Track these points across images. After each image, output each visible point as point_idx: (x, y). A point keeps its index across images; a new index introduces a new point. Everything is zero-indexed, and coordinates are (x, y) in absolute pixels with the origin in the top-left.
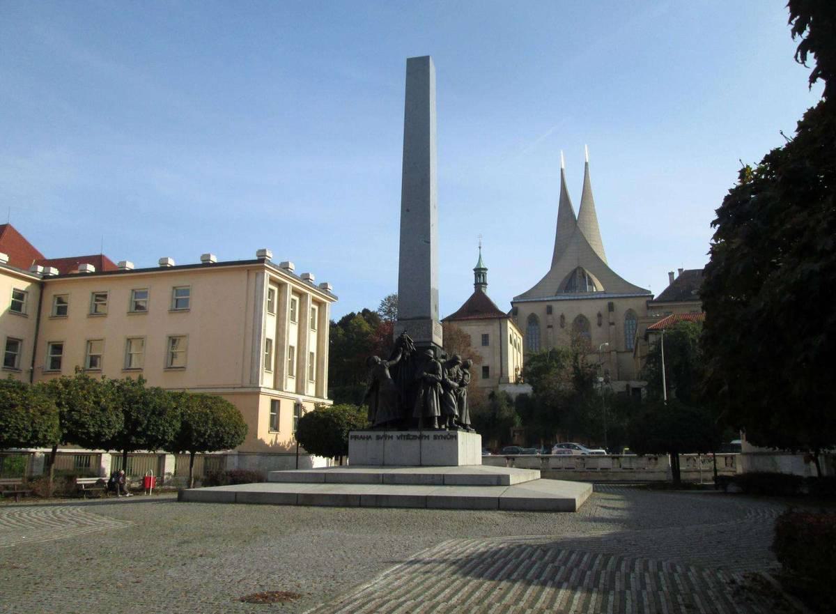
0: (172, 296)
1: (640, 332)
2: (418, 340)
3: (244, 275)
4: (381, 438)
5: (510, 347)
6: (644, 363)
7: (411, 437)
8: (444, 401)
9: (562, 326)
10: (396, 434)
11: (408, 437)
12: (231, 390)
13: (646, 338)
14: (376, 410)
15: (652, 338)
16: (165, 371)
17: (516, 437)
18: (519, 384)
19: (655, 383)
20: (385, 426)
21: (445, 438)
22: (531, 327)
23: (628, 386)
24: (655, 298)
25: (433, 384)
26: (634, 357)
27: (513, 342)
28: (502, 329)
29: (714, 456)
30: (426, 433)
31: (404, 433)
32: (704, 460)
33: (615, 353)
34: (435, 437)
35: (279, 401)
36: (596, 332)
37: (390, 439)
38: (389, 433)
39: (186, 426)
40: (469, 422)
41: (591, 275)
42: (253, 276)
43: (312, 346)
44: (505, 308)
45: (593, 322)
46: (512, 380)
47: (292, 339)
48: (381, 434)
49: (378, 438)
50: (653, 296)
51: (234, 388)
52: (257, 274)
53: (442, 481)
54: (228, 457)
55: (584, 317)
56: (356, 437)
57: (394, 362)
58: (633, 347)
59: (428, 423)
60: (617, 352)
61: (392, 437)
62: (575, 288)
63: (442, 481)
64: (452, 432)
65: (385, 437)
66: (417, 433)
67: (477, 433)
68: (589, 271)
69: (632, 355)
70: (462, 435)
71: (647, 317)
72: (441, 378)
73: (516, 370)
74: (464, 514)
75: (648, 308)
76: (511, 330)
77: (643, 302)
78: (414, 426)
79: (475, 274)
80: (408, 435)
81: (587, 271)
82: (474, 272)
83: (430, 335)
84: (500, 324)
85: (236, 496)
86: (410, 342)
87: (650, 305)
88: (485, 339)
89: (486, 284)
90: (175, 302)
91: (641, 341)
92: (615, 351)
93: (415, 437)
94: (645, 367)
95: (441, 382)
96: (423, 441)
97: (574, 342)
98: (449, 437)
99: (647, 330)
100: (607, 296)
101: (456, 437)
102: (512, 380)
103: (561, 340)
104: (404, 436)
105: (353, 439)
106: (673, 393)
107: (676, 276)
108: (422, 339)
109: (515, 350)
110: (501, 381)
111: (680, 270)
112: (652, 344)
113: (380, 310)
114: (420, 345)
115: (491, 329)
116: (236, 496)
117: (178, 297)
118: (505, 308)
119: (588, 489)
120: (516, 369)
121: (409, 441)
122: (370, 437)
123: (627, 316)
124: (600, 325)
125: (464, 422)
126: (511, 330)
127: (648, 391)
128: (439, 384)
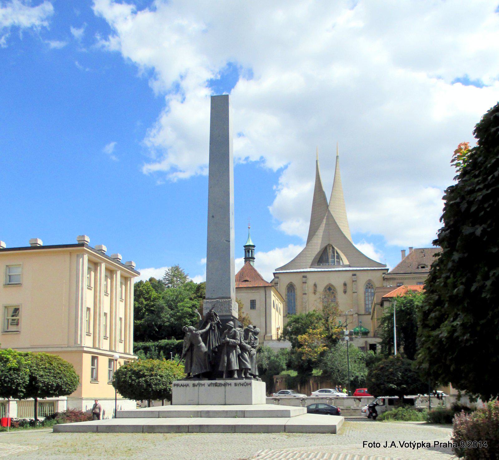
0: (6, 273)
1: (377, 300)
2: (221, 314)
3: (67, 258)
4: (197, 386)
5: (273, 311)
6: (380, 324)
7: (218, 385)
8: (240, 357)
9: (315, 293)
10: (207, 382)
11: (216, 385)
12: (60, 349)
13: (382, 305)
14: (191, 366)
15: (386, 304)
16: (3, 334)
17: (278, 384)
18: (281, 341)
19: (388, 343)
20: (198, 377)
21: (242, 385)
22: (290, 296)
23: (366, 342)
24: (389, 271)
25: (234, 347)
26: (372, 319)
27: (275, 307)
28: (267, 296)
29: (430, 397)
30: (229, 381)
31: (213, 382)
32: (423, 400)
33: (357, 315)
34: (236, 385)
35: (97, 357)
36: (341, 298)
37: (230, 386)
38: (202, 382)
39: (33, 379)
40: (257, 374)
41: (339, 251)
42: (74, 257)
43: (121, 314)
44: (268, 277)
45: (340, 289)
46: (274, 337)
47: (106, 308)
48: (197, 382)
49: (194, 385)
50: (388, 270)
51: (62, 347)
52: (78, 256)
53: (243, 414)
54: (59, 402)
55: (332, 286)
56: (177, 385)
57: (204, 330)
58: (371, 311)
59: (230, 374)
60: (359, 315)
61: (231, 384)
62: (327, 261)
63: (243, 414)
64: (248, 381)
65: (199, 385)
67: (263, 381)
68: (338, 248)
69: (370, 317)
70: (254, 382)
71: (383, 287)
72: (239, 342)
73: (278, 329)
74: (263, 436)
75: (384, 279)
76: (274, 298)
77: (379, 275)
78: (219, 376)
79: (245, 250)
80: (216, 383)
81: (335, 248)
82: (244, 248)
83: (230, 310)
84: (265, 292)
85: (97, 428)
86: (216, 316)
87: (386, 276)
89: (254, 258)
90: (8, 277)
91: (378, 307)
92: (356, 313)
93: (220, 385)
94: (380, 327)
95: (239, 345)
96: (227, 387)
97: (325, 307)
98: (245, 384)
99: (383, 298)
101: (250, 384)
102: (274, 337)
103: (311, 304)
104: (213, 384)
105: (176, 387)
106: (402, 350)
107: (407, 253)
108: (225, 314)
109: (277, 313)
110: (266, 338)
111: (411, 248)
112: (386, 308)
113: (164, 279)
114: (224, 318)
115: (258, 296)
116: (97, 428)
117: (11, 274)
118: (268, 277)
119: (341, 419)
120: (277, 328)
121: (216, 387)
122: (188, 385)
123: (367, 286)
124: (345, 292)
125: (254, 374)
126: (274, 298)
127: (382, 347)
128: (238, 347)
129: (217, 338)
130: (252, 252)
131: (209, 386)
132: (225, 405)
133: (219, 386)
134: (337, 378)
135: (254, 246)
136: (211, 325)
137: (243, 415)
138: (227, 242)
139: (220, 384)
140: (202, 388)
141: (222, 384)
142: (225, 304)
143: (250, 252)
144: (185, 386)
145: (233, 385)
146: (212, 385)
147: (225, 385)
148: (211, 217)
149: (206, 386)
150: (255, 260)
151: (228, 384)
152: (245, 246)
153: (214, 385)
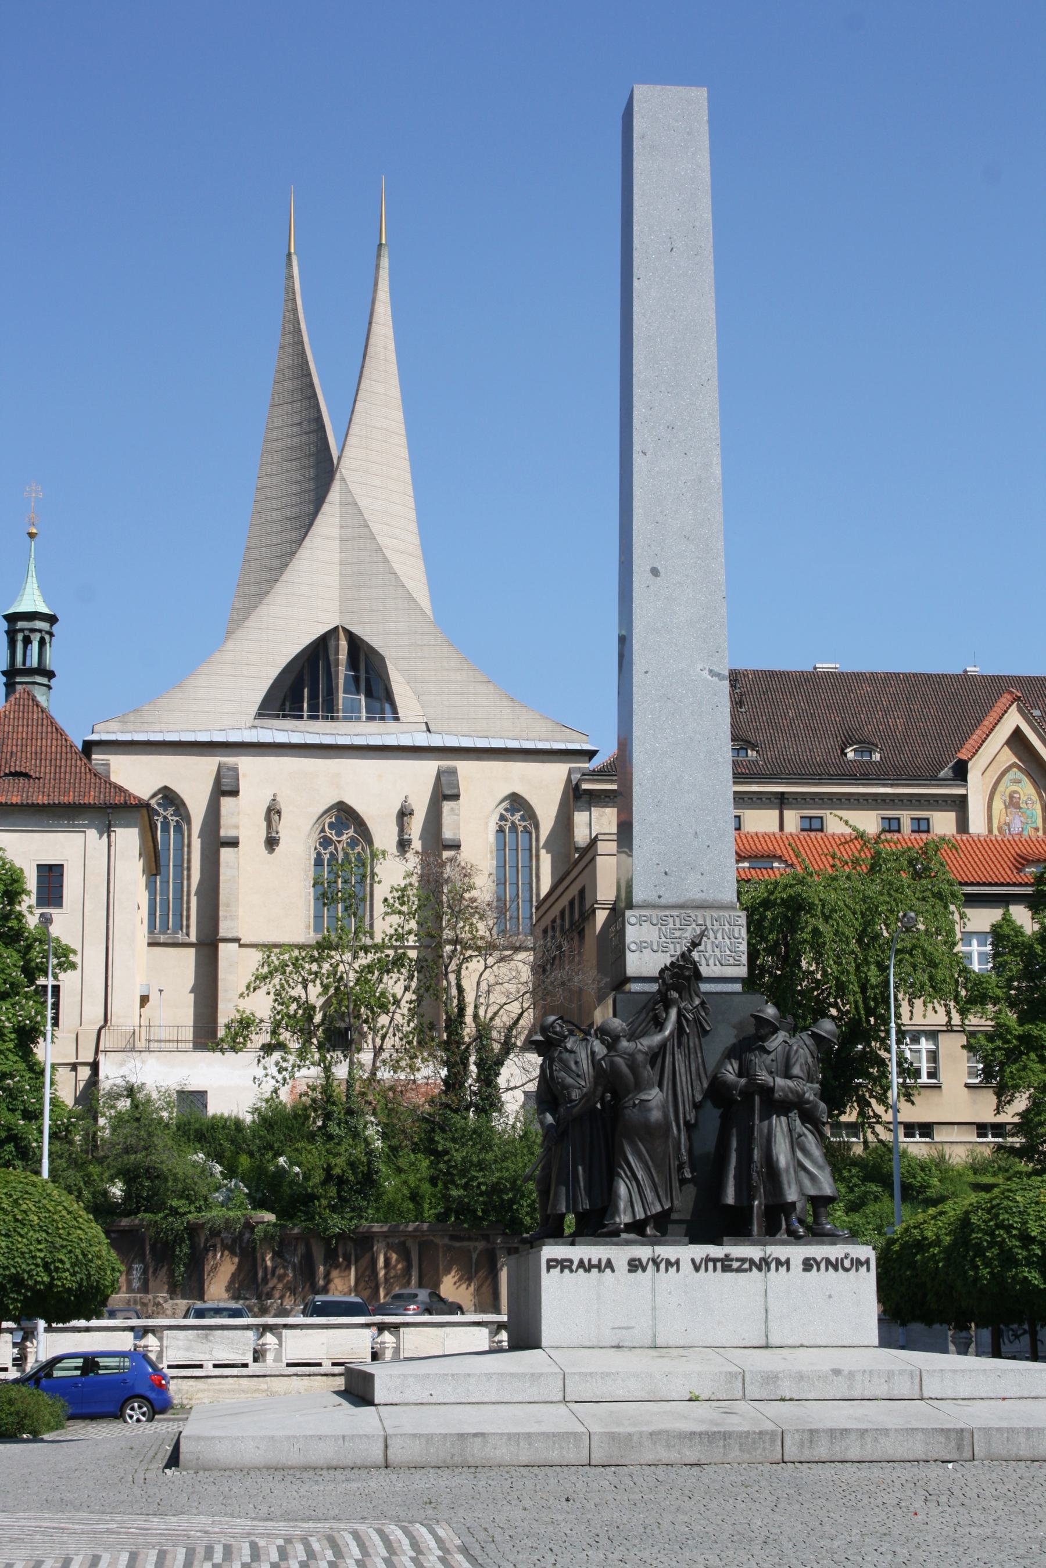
11: (726, 1265)
21: (836, 1269)
34: (808, 1265)
38: (666, 1252)
48: (644, 1252)
49: (635, 1265)
66: (754, 1252)
88: (51, 878)
98: (847, 1264)
100: (436, 741)
104: (715, 1261)
105: (555, 1272)
122: (609, 1264)
124: (272, 843)
129: (698, 1069)
130: (42, 643)
131: (697, 1269)
132: (767, 1347)
133: (738, 1270)
134: (398, 1261)
135: (52, 619)
136: (680, 1014)
137: (917, 1387)
138: (715, 679)
139: (743, 1260)
140: (776, 1277)
141: (752, 1262)
142: (715, 933)
143: (35, 645)
144: (595, 1271)
145: (797, 1264)
146: (711, 1265)
147: (763, 1265)
148: (621, 563)
149: (686, 1266)
150: (53, 682)
151: (779, 1263)
152: (7, 617)
153: (719, 1265)
